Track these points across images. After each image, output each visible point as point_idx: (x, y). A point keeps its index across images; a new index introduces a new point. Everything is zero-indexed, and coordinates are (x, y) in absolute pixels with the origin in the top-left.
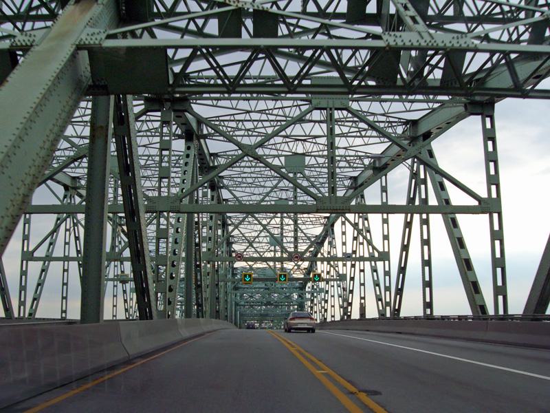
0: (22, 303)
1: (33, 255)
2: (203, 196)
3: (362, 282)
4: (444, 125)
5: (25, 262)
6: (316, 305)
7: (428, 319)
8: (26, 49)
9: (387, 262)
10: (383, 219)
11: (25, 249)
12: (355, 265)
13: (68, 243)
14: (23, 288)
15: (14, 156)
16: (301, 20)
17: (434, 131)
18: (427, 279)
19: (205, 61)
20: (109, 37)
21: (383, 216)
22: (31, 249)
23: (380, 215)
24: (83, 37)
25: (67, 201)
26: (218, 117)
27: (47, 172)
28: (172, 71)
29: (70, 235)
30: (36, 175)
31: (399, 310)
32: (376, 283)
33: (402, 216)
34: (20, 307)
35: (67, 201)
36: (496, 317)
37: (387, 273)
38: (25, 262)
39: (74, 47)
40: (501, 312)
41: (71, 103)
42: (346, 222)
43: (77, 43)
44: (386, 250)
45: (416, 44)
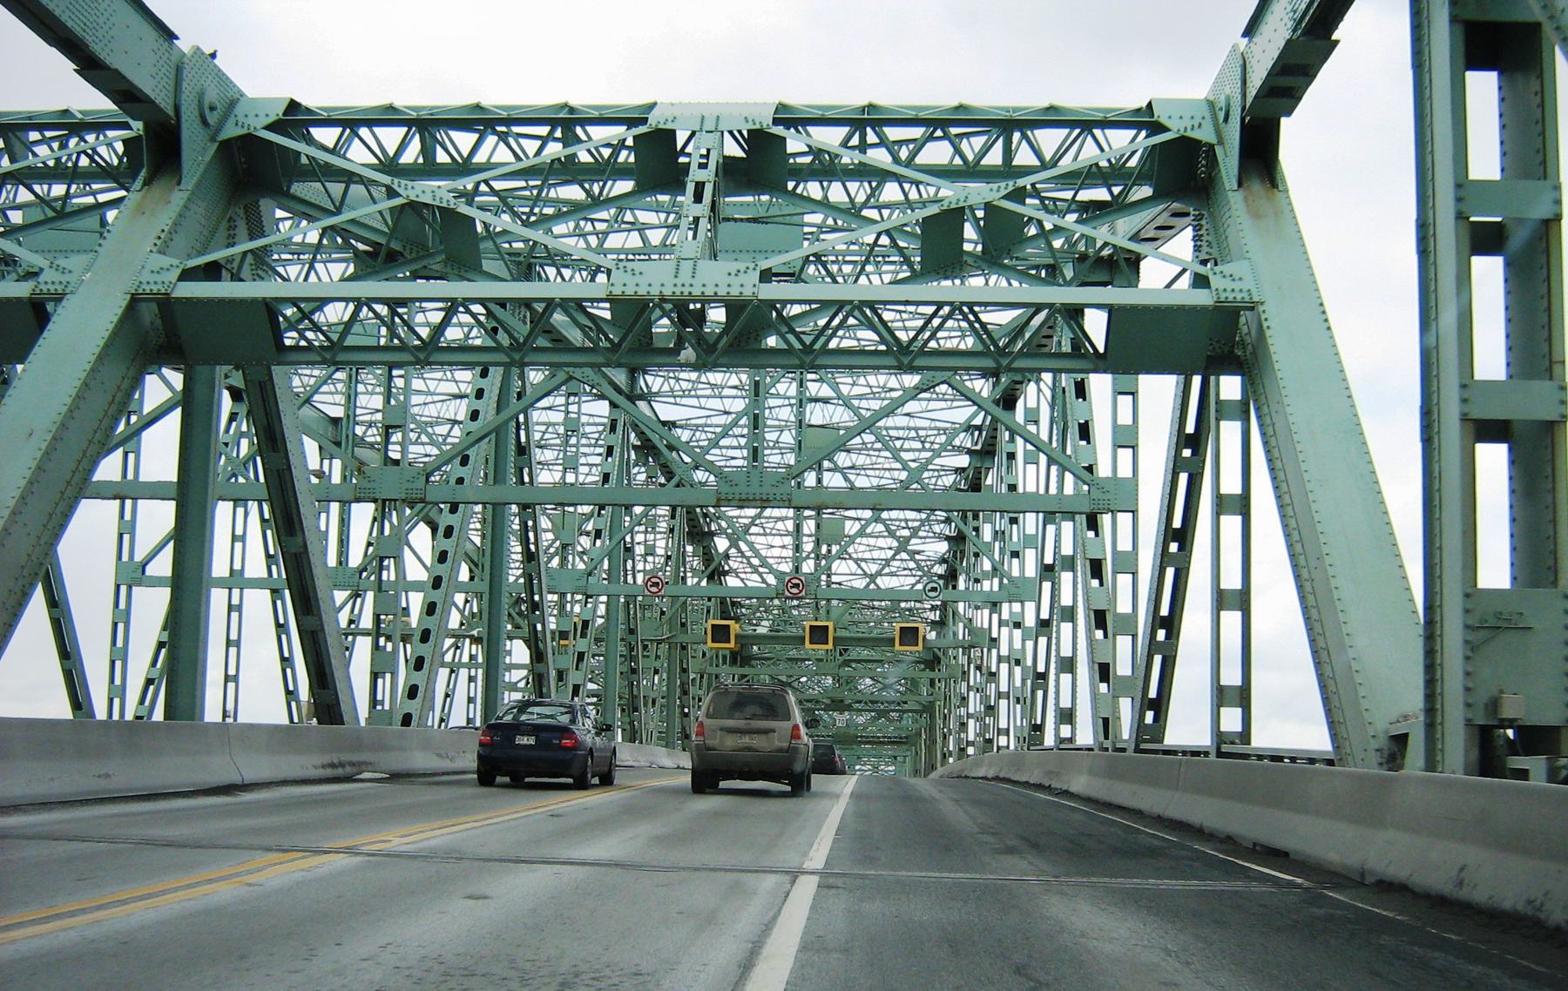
0: (117, 692)
1: (143, 572)
2: (713, 386)
3: (1231, 676)
4: (1462, 193)
5: (123, 589)
8: (58, 298)
11: (125, 558)
13: (243, 539)
14: (119, 655)
17: (68, 664)
20: (187, 275)
22: (138, 557)
24: (144, 278)
25: (239, 426)
29: (246, 514)
30: (102, 441)
34: (111, 701)
35: (239, 426)
36: (108, 723)
38: (123, 589)
39: (129, 297)
40: (116, 717)
41: (132, 373)
43: (208, 137)
44: (1125, 471)
45: (722, 292)
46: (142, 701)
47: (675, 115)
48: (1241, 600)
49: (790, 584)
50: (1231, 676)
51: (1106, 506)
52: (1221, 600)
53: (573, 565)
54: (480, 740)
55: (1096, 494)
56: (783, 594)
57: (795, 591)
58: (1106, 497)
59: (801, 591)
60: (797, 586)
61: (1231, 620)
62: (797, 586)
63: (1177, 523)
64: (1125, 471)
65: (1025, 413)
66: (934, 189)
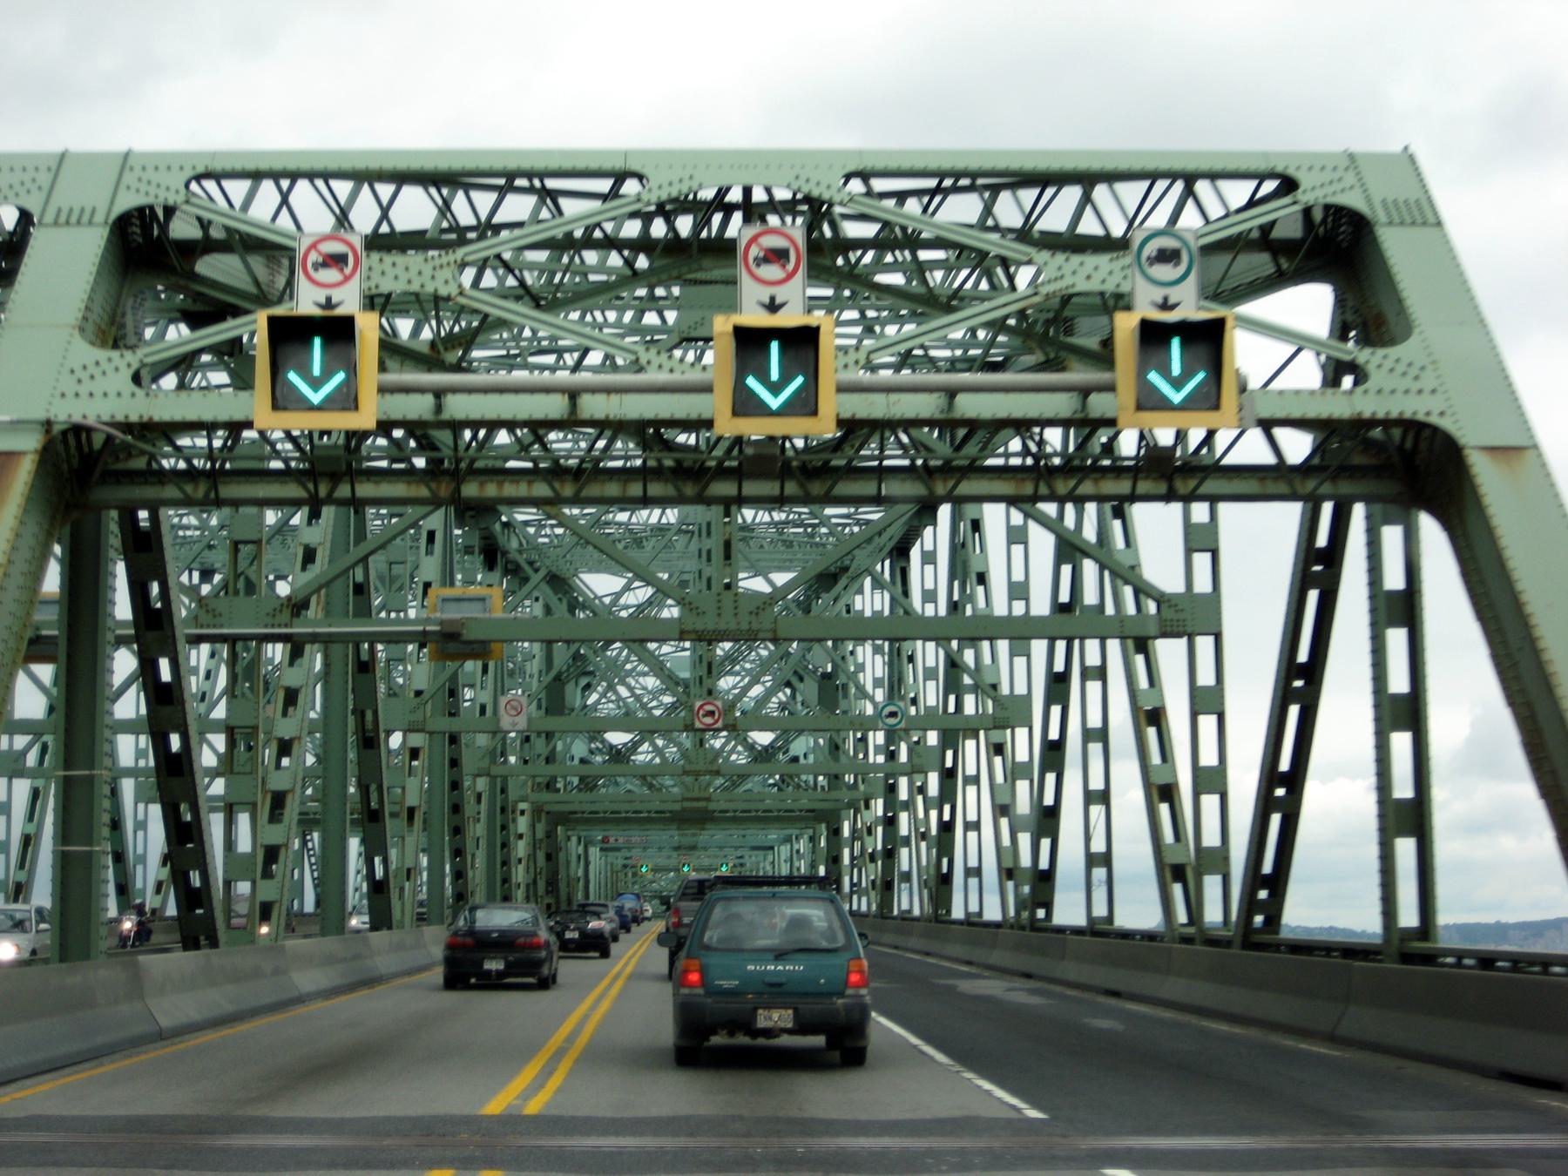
3: (1098, 846)
6: (906, 841)
7: (1407, 958)
9: (1205, 644)
10: (1189, 527)
12: (1011, 598)
15: (108, 391)
16: (974, 219)
18: (1403, 789)
19: (1104, 807)
21: (1187, 515)
23: (1176, 508)
26: (542, 175)
27: (459, 577)
28: (1183, 925)
31: (1278, 882)
32: (1159, 779)
33: (1289, 514)
37: (1207, 701)
42: (1032, 525)
44: (1203, 584)
46: (31, 818)
47: (288, 719)
48: (1104, 797)
49: (701, 712)
50: (1098, 846)
51: (1181, 629)
52: (1090, 798)
53: (182, 269)
54: (151, 208)
55: (1168, 613)
56: (693, 724)
57: (709, 720)
58: (1180, 616)
59: (717, 721)
60: (711, 714)
61: (1097, 811)
62: (711, 714)
63: (1303, 656)
64: (1203, 584)
65: (922, 556)
66: (483, 284)
